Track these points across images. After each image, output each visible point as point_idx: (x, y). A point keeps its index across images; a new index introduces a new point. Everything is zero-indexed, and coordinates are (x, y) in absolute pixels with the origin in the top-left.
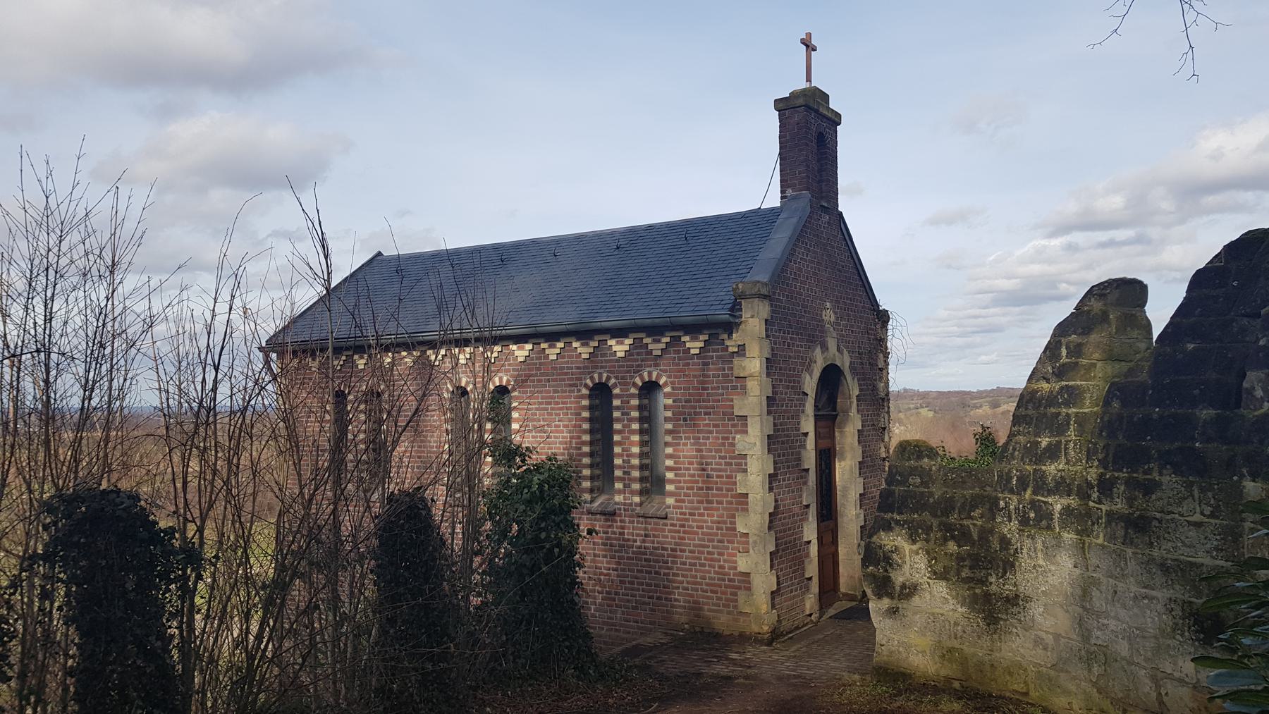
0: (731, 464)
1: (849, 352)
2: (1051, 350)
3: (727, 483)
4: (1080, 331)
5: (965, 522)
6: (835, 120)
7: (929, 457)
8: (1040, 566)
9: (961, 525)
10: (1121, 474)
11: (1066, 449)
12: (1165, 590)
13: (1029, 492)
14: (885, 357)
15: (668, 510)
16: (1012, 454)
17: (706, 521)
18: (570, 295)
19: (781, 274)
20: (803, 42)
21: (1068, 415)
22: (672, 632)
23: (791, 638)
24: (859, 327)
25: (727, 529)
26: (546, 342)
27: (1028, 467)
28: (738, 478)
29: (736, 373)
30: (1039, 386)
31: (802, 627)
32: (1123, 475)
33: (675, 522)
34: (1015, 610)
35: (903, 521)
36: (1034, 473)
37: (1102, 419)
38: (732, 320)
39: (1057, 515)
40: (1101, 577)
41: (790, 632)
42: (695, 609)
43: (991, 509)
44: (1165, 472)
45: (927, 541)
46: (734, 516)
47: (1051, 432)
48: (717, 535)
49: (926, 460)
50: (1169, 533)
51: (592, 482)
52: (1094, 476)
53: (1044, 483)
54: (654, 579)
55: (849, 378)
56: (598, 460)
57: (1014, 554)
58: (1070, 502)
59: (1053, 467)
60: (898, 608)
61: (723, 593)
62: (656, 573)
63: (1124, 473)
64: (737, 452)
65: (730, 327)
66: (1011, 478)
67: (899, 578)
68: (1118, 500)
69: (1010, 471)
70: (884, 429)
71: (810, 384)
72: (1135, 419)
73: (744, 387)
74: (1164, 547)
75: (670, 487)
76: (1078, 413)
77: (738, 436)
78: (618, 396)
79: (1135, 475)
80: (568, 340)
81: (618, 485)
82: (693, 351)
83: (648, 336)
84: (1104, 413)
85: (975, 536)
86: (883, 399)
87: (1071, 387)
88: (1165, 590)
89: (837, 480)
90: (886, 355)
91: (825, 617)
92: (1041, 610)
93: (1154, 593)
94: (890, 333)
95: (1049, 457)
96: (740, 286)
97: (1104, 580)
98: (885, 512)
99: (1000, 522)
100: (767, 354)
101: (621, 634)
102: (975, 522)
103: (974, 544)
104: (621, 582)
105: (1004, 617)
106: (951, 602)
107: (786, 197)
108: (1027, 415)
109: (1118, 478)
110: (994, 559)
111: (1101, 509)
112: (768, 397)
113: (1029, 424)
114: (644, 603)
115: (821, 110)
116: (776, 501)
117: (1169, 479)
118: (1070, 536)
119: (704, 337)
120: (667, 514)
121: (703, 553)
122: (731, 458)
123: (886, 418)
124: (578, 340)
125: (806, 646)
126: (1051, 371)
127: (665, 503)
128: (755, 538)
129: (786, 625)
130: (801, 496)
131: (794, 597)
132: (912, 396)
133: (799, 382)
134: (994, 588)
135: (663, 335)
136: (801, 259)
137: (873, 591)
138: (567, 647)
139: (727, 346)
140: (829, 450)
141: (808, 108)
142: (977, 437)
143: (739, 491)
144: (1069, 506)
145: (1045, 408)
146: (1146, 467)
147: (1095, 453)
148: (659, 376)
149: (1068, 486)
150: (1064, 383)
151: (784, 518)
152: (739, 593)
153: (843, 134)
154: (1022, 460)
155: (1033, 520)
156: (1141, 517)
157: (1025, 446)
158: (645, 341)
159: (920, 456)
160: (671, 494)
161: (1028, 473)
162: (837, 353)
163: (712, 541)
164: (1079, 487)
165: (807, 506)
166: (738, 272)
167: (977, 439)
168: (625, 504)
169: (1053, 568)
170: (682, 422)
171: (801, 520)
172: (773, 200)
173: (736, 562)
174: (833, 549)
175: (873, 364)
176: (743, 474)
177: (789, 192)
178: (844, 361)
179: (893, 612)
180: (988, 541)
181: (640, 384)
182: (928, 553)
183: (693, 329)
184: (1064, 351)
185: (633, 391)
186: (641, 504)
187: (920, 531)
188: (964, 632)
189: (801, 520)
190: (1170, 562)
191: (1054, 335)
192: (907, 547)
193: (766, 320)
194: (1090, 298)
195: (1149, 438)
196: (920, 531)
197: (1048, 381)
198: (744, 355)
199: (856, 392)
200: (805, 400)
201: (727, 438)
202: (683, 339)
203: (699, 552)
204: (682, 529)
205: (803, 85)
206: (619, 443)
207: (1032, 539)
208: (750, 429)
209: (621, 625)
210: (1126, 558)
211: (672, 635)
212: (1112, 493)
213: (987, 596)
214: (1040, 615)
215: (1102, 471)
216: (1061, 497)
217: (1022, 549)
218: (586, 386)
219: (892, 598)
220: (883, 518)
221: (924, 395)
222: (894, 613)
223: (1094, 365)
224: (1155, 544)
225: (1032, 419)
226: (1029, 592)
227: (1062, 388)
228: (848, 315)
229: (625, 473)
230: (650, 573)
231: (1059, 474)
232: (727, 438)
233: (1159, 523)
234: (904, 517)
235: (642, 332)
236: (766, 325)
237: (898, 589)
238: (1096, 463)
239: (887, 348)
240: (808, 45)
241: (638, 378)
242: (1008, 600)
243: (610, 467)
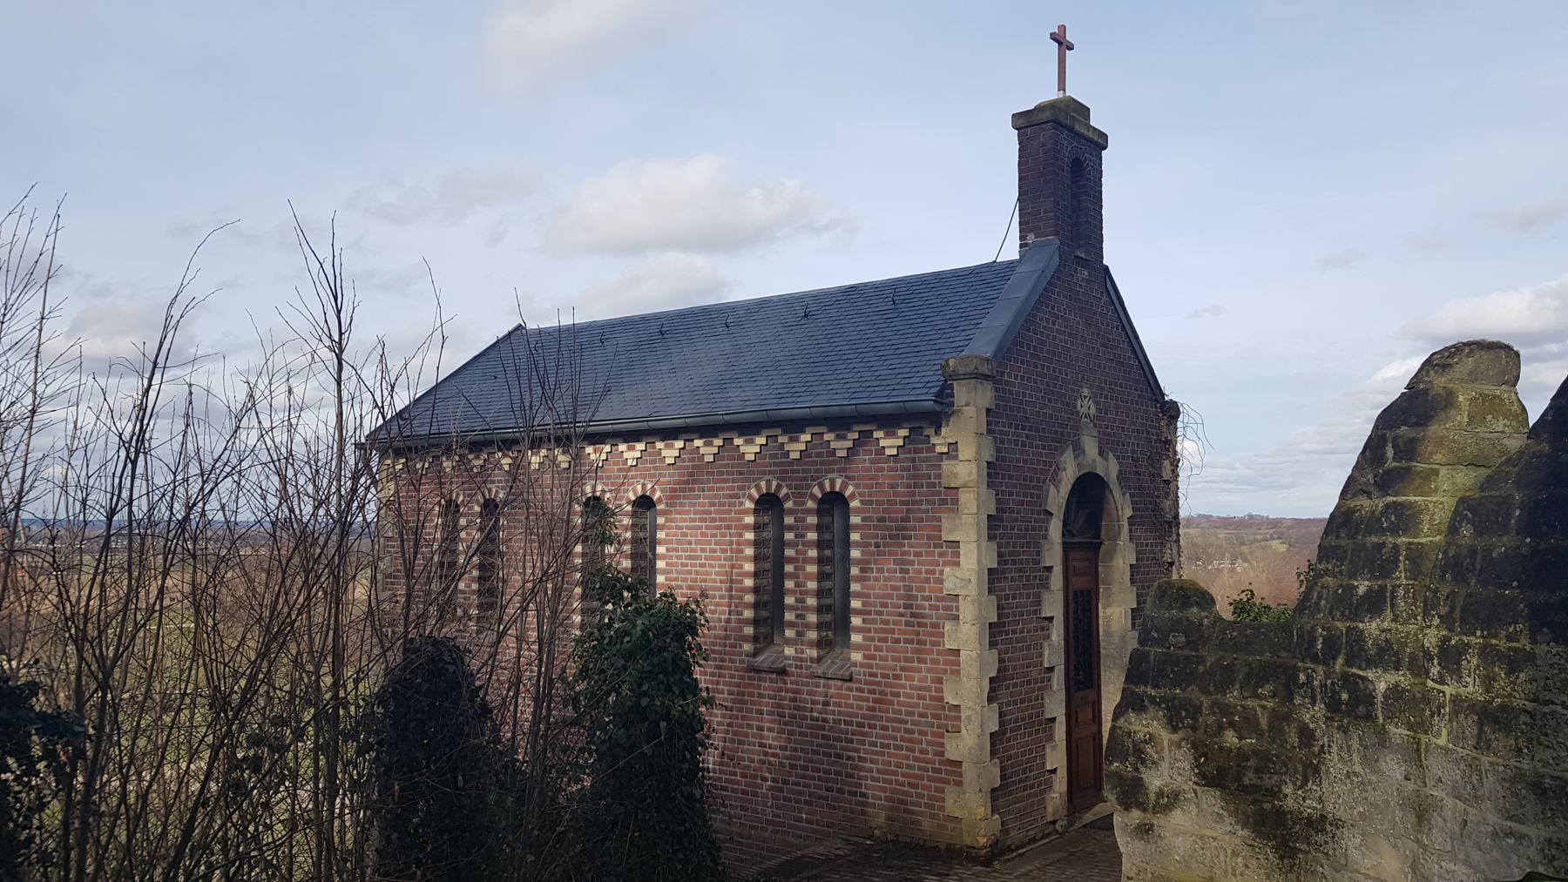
0: (937, 608)
1: (1118, 458)
2: (1373, 450)
3: (932, 635)
4: (1414, 419)
5: (1249, 703)
6: (1099, 142)
7: (1199, 605)
8: (1355, 774)
9: (1242, 706)
10: (1472, 638)
11: (1393, 597)
12: (1541, 826)
13: (1340, 660)
14: (1172, 465)
15: (853, 669)
16: (1317, 603)
17: (903, 687)
18: (735, 376)
19: (1012, 347)
20: (1054, 37)
21: (1396, 547)
22: (856, 839)
23: (1020, 855)
24: (1134, 424)
25: (932, 698)
26: (700, 438)
27: (1339, 624)
28: (946, 628)
29: (945, 483)
30: (1359, 503)
31: (1041, 839)
32: (1476, 640)
33: (863, 686)
34: (1320, 838)
35: (1160, 698)
36: (1347, 632)
37: (1445, 553)
38: (938, 408)
39: (1380, 698)
40: (1444, 796)
41: (1022, 847)
42: (899, 806)
43: (1287, 685)
44: (1539, 638)
45: (1194, 728)
46: (940, 681)
47: (1371, 571)
48: (917, 706)
49: (1195, 610)
50: (1546, 735)
51: (755, 628)
52: (1434, 640)
53: (1362, 649)
54: (834, 763)
55: (1116, 492)
56: (765, 598)
57: (1319, 754)
58: (1398, 679)
59: (1374, 625)
60: (1152, 825)
61: (925, 788)
62: (838, 756)
63: (1477, 638)
64: (945, 592)
65: (937, 418)
66: (1315, 640)
67: (1155, 781)
68: (1468, 679)
69: (1313, 629)
70: (1171, 564)
71: (1057, 498)
72: (1494, 555)
73: (956, 501)
74: (1537, 757)
75: (856, 638)
76: (1410, 543)
77: (947, 569)
78: (791, 512)
79: (1494, 641)
80: (728, 436)
81: (789, 633)
82: (888, 452)
83: (830, 431)
84: (1449, 544)
85: (1264, 723)
86: (1170, 523)
87: (1401, 504)
88: (1541, 826)
89: (1101, 634)
90: (1175, 464)
91: (1078, 825)
92: (1358, 841)
93: (1523, 829)
94: (1180, 432)
95: (1369, 611)
96: (951, 362)
97: (1449, 802)
98: (1136, 684)
99: (1300, 705)
100: (988, 454)
101: (789, 838)
102: (1264, 702)
103: (1262, 735)
104: (793, 766)
105: (1304, 847)
106: (1228, 820)
107: (1026, 245)
108: (1338, 547)
109: (1468, 645)
110: (1290, 759)
111: (1443, 692)
112: (988, 516)
113: (1342, 559)
114: (820, 797)
115: (1077, 127)
116: (1001, 661)
117: (1546, 649)
118: (1399, 731)
119: (903, 432)
120: (851, 675)
121: (898, 730)
122: (938, 599)
123: (1175, 551)
124: (740, 435)
125: (1038, 869)
126: (1372, 481)
127: (850, 659)
128: (970, 712)
129: (1016, 835)
130: (1041, 655)
131: (1029, 796)
132: (1259, 525)
133: (1038, 497)
134: (1290, 803)
135: (849, 429)
136: (1044, 327)
137: (1117, 799)
138: (680, 862)
139: (934, 445)
140: (1089, 591)
141: (1057, 123)
142: (1302, 578)
143: (947, 647)
144: (1397, 685)
145: (1364, 536)
146: (1511, 630)
147: (1435, 606)
148: (844, 486)
149: (1396, 654)
150: (1391, 499)
151: (1015, 685)
152: (947, 788)
153: (1112, 163)
154: (1331, 613)
155: (1346, 704)
156: (1503, 707)
157: (1335, 592)
158: (827, 437)
159: (1185, 605)
160: (858, 647)
161: (1338, 633)
162: (1098, 459)
163: (912, 714)
164: (1413, 657)
165: (1051, 669)
166: (954, 345)
167: (1302, 581)
168: (796, 659)
169: (1374, 779)
170: (873, 548)
171: (1040, 689)
172: (1011, 252)
173: (942, 745)
174: (1094, 728)
175: (1155, 475)
176: (954, 622)
177: (1031, 238)
178: (1109, 469)
179: (1145, 831)
180: (1282, 732)
181: (820, 496)
182: (1194, 746)
183: (889, 421)
184: (1390, 452)
185: (811, 504)
186: (819, 660)
187: (1184, 713)
188: (1247, 867)
189: (1040, 689)
190: (1548, 781)
191: (1376, 427)
192: (1166, 736)
193: (988, 410)
194: (1428, 372)
195: (1515, 584)
196: (1184, 713)
197: (1369, 495)
198: (956, 457)
199: (1129, 512)
200: (1048, 521)
201: (933, 572)
202: (876, 434)
203: (894, 729)
204: (871, 696)
205: (1052, 94)
206: (792, 576)
207: (1344, 732)
208: (962, 560)
209: (790, 826)
210: (1480, 771)
211: (855, 844)
212: (1459, 669)
213: (1280, 815)
214: (1355, 848)
215: (1445, 633)
216: (1385, 670)
217: (1329, 746)
218: (750, 497)
219: (1145, 810)
220: (1133, 692)
221: (1276, 523)
222: (1147, 832)
223: (1436, 473)
224: (1525, 751)
225: (1346, 552)
226: (1341, 813)
227: (1387, 506)
228: (1118, 407)
229: (798, 616)
230: (828, 755)
231: (1383, 635)
232: (933, 572)
233: (1531, 717)
234: (1161, 692)
235: (822, 425)
236: (988, 415)
237: (1152, 796)
238: (1436, 621)
239: (1175, 453)
240: (1062, 42)
241: (816, 487)
242: (1310, 822)
243: (781, 608)
